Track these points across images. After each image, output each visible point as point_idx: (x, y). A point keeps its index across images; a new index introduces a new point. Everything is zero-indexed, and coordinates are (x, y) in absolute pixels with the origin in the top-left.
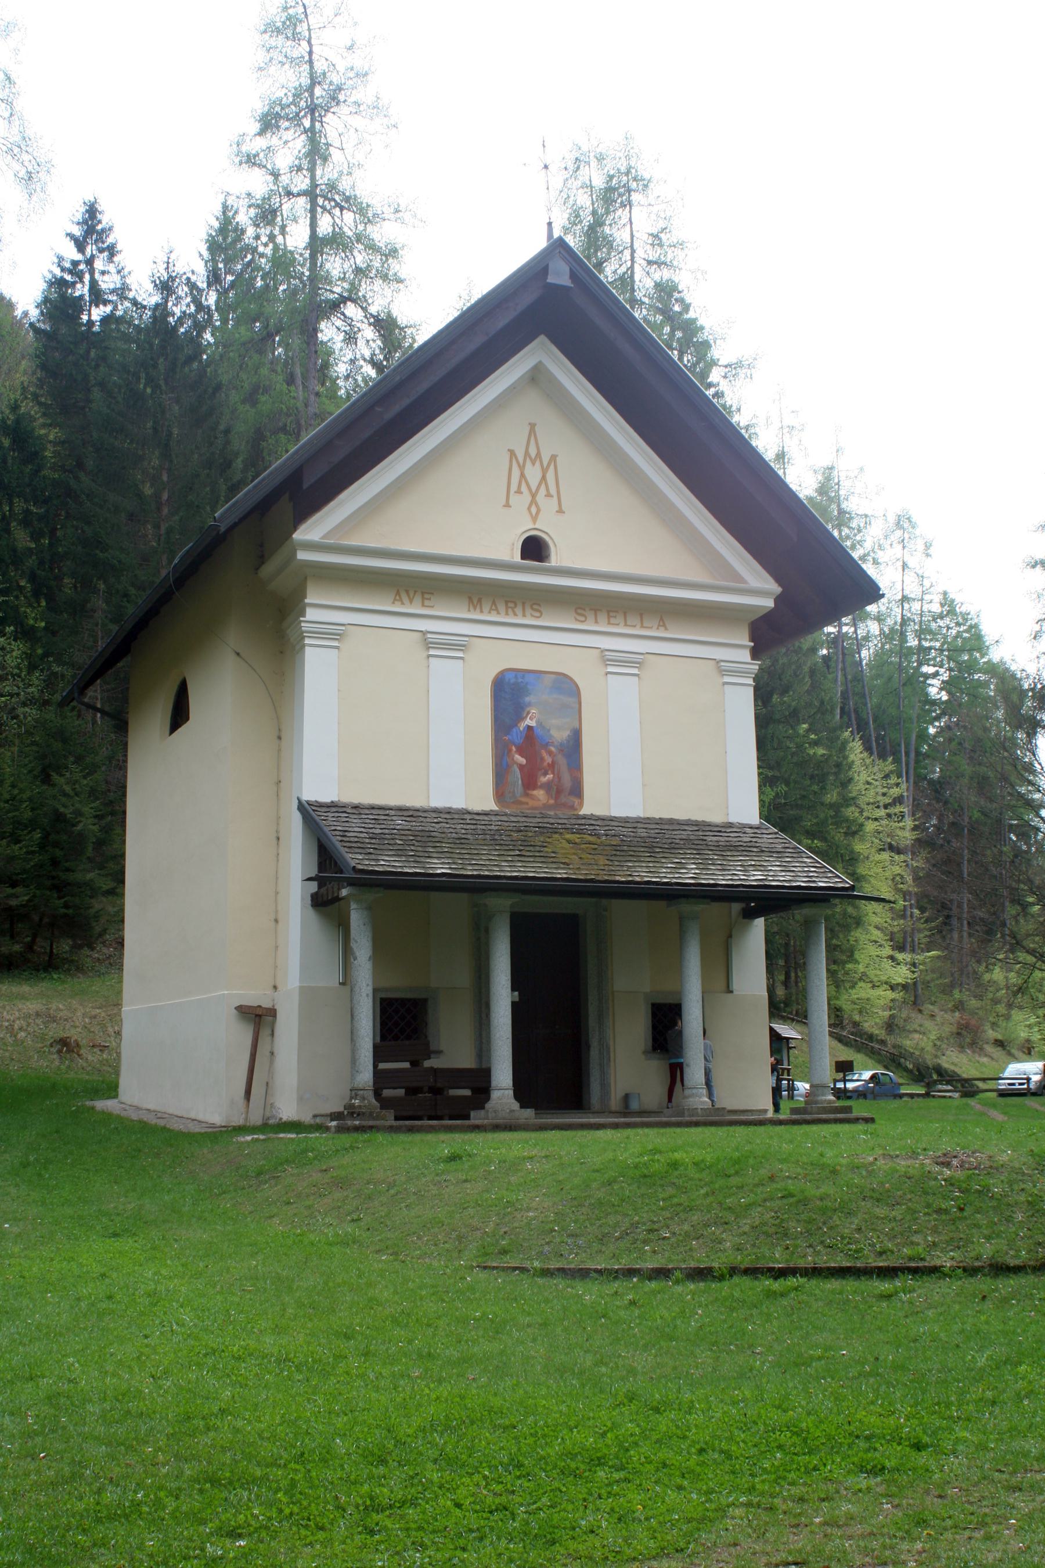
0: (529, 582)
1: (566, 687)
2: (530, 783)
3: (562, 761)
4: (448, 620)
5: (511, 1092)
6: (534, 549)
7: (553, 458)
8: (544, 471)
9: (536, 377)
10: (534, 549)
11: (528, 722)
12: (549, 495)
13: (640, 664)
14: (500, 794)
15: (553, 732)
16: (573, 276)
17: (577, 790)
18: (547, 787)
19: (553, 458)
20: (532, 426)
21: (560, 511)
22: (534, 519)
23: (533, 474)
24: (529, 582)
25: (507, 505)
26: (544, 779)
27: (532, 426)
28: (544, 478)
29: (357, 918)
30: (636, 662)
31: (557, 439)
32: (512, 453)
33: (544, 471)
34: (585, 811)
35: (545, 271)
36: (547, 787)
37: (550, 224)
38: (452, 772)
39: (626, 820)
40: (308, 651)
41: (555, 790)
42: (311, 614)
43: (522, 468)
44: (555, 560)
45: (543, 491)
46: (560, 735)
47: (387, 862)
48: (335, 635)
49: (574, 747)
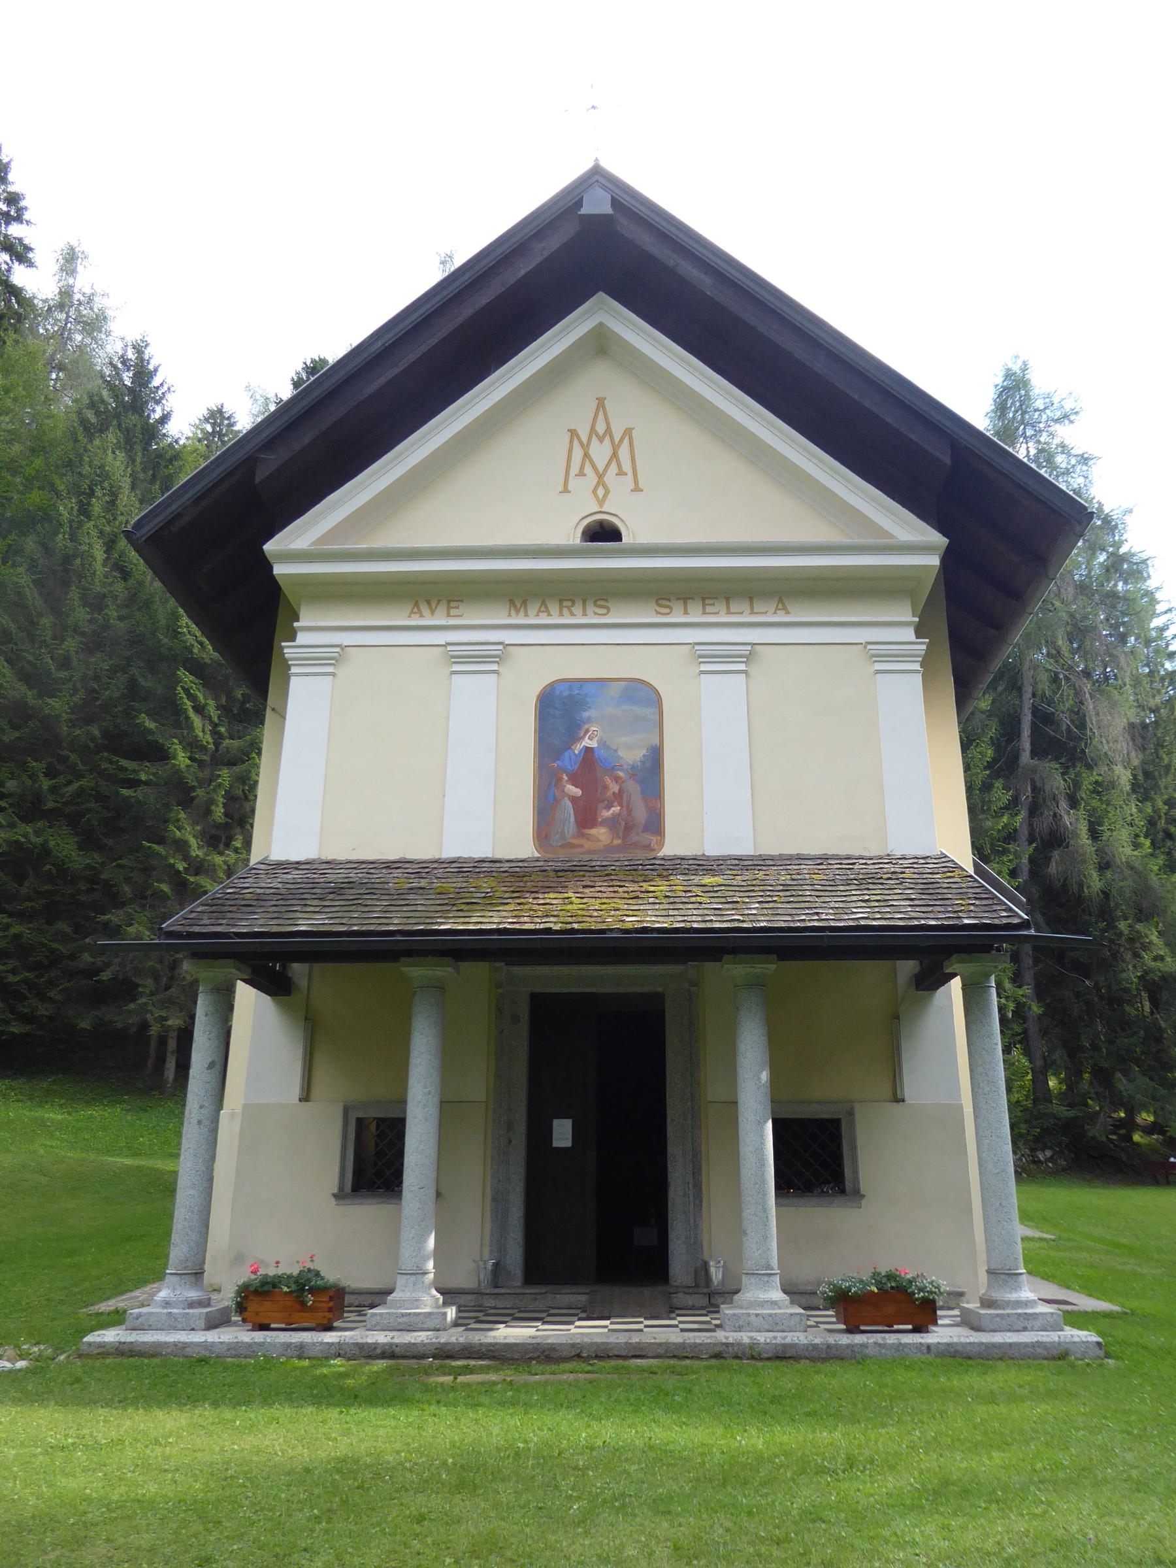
1: (643, 696)
2: (586, 817)
3: (633, 788)
4: (482, 625)
7: (628, 432)
11: (587, 742)
14: (542, 834)
17: (655, 824)
19: (628, 432)
20: (601, 402)
22: (601, 502)
23: (600, 453)
24: (599, 574)
25: (566, 490)
27: (601, 402)
28: (615, 455)
31: (631, 408)
32: (573, 433)
36: (612, 823)
41: (624, 827)
43: (585, 448)
46: (630, 752)
48: (335, 658)
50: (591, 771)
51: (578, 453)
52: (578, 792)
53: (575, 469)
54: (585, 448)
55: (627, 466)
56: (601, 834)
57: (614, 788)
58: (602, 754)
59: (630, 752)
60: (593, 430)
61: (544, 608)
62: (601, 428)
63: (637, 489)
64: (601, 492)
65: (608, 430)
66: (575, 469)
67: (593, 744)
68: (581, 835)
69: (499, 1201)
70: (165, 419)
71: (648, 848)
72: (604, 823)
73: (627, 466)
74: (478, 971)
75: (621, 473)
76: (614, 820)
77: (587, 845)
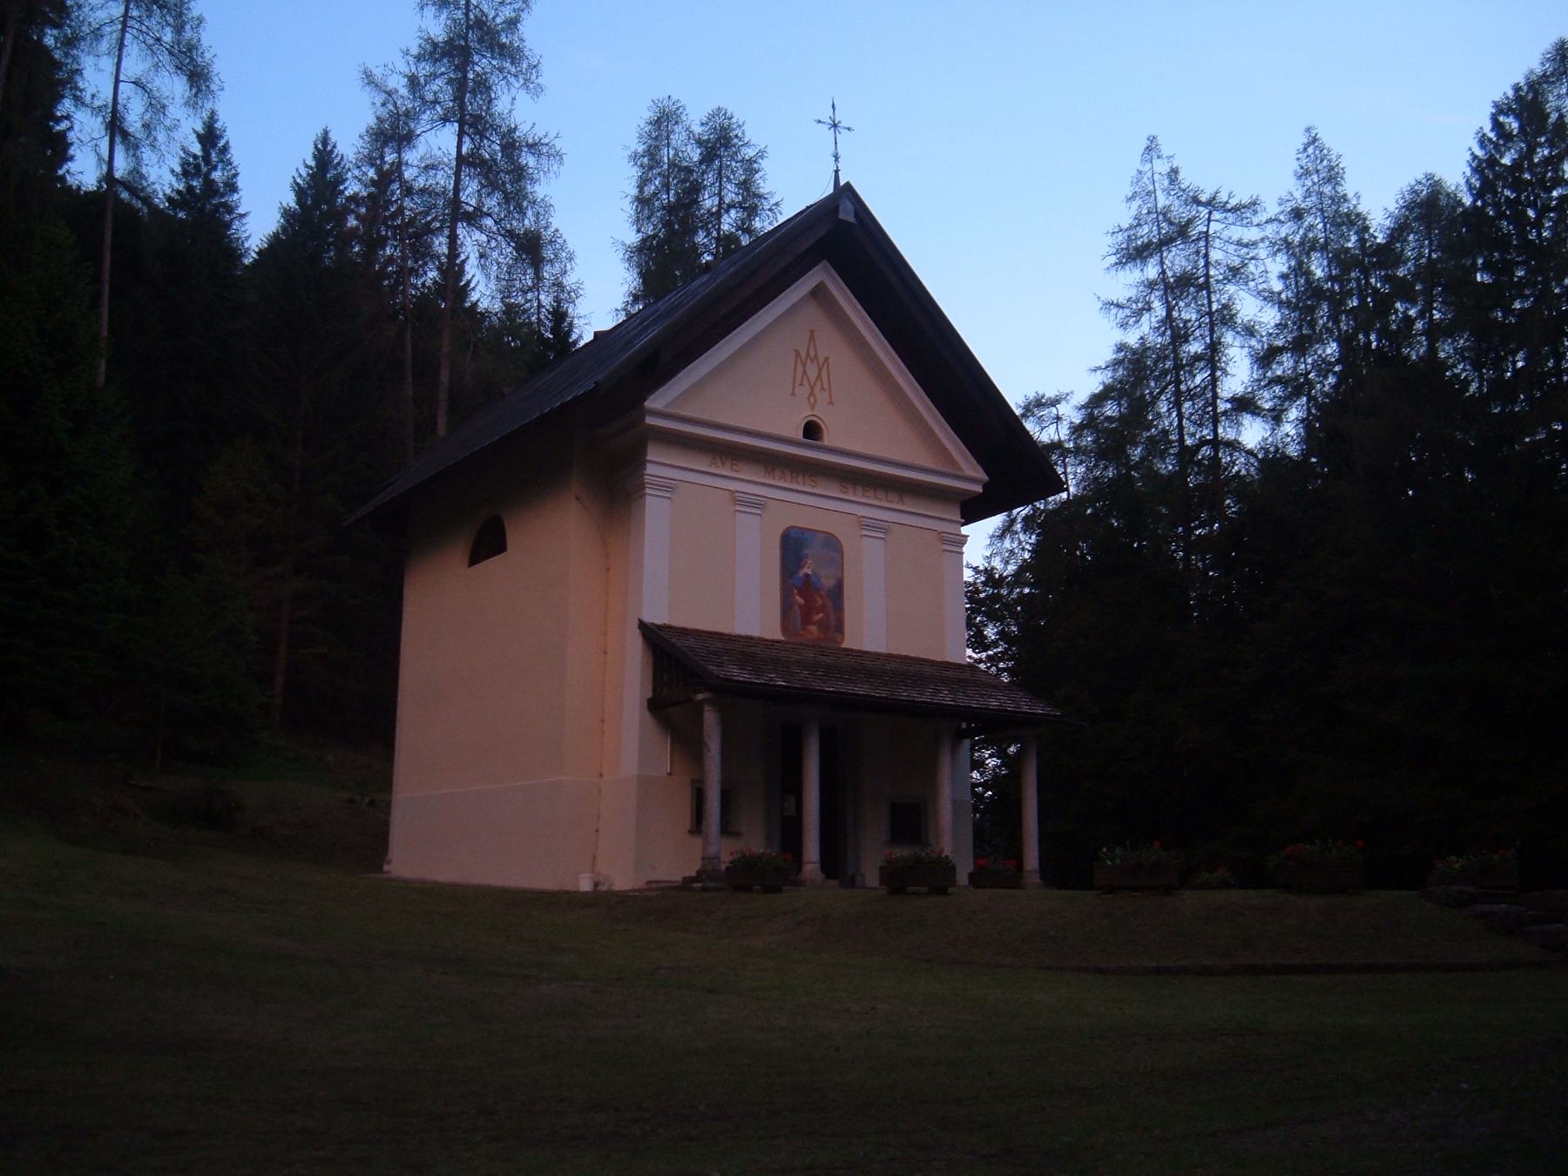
0: (803, 461)
1: (832, 544)
2: (807, 620)
3: (830, 604)
4: (749, 482)
5: (818, 866)
6: (812, 431)
7: (827, 359)
8: (820, 370)
9: (819, 293)
10: (812, 431)
11: (807, 570)
12: (822, 389)
13: (886, 531)
14: (785, 629)
15: (824, 580)
16: (856, 215)
17: (840, 628)
18: (819, 623)
19: (827, 359)
20: (812, 332)
21: (831, 403)
22: (813, 408)
23: (812, 371)
24: (803, 461)
25: (793, 394)
26: (818, 617)
27: (812, 332)
28: (819, 375)
29: (710, 718)
30: (883, 528)
31: (831, 345)
32: (797, 352)
33: (820, 370)
34: (845, 645)
35: (836, 209)
36: (819, 623)
37: (837, 172)
38: (752, 611)
39: (877, 656)
40: (648, 498)
41: (824, 626)
42: (650, 469)
43: (804, 365)
44: (828, 440)
45: (818, 386)
46: (828, 582)
47: (740, 675)
48: (670, 487)
49: (837, 593)
51: (800, 368)
56: (813, 628)
59: (828, 582)
70: (247, 238)
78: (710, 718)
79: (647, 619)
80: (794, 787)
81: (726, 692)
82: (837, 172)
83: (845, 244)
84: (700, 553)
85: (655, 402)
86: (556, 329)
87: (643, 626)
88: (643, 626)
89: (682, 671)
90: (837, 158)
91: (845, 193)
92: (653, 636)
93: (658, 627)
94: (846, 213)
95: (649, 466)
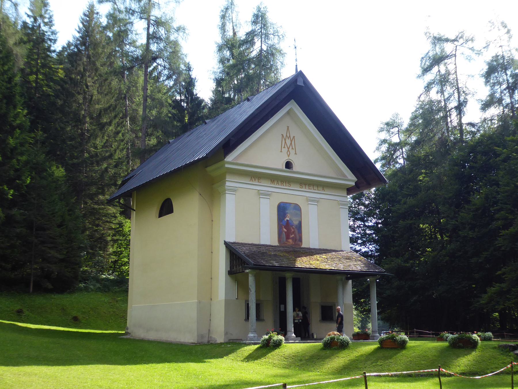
0: (286, 176)
1: (297, 208)
2: (288, 237)
3: (296, 232)
4: (265, 187)
6: (288, 165)
7: (294, 137)
8: (291, 141)
10: (288, 165)
12: (292, 149)
13: (318, 202)
14: (279, 241)
17: (301, 240)
19: (294, 137)
20: (288, 127)
21: (296, 154)
22: (289, 156)
24: (286, 176)
25: (281, 151)
27: (288, 127)
28: (291, 143)
29: (251, 280)
30: (317, 201)
31: (295, 132)
32: (282, 135)
36: (292, 238)
37: (296, 66)
38: (267, 235)
41: (294, 239)
42: (228, 184)
43: (285, 140)
44: (296, 167)
46: (296, 223)
48: (234, 190)
49: (299, 226)
50: (288, 224)
52: (286, 230)
53: (283, 146)
54: (285, 140)
55: (294, 147)
56: (290, 240)
57: (293, 230)
58: (290, 221)
60: (287, 136)
61: (278, 183)
62: (288, 136)
63: (296, 154)
64: (288, 153)
65: (290, 136)
66: (283, 146)
67: (288, 219)
68: (287, 241)
69: (275, 321)
71: (299, 245)
72: (291, 239)
73: (294, 147)
74: (269, 273)
75: (292, 149)
76: (293, 238)
77: (288, 244)
78: (251, 280)
79: (227, 240)
80: (283, 300)
81: (258, 268)
82: (296, 66)
83: (300, 93)
84: (247, 216)
85: (230, 158)
86: (243, 343)
87: (226, 243)
88: (226, 243)
89: (240, 260)
90: (296, 60)
91: (300, 75)
92: (227, 245)
93: (232, 243)
94: (300, 83)
95: (227, 182)
